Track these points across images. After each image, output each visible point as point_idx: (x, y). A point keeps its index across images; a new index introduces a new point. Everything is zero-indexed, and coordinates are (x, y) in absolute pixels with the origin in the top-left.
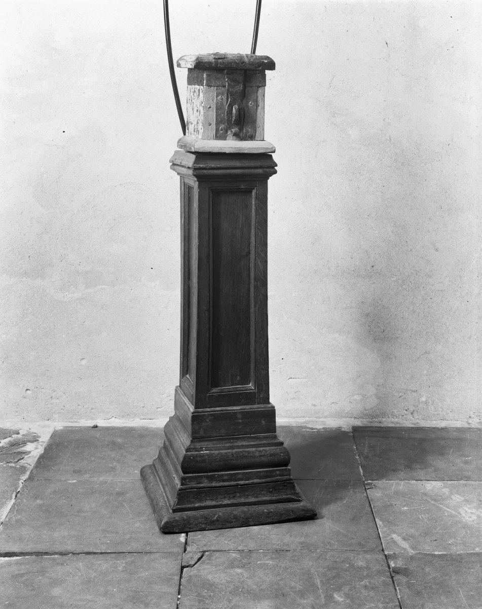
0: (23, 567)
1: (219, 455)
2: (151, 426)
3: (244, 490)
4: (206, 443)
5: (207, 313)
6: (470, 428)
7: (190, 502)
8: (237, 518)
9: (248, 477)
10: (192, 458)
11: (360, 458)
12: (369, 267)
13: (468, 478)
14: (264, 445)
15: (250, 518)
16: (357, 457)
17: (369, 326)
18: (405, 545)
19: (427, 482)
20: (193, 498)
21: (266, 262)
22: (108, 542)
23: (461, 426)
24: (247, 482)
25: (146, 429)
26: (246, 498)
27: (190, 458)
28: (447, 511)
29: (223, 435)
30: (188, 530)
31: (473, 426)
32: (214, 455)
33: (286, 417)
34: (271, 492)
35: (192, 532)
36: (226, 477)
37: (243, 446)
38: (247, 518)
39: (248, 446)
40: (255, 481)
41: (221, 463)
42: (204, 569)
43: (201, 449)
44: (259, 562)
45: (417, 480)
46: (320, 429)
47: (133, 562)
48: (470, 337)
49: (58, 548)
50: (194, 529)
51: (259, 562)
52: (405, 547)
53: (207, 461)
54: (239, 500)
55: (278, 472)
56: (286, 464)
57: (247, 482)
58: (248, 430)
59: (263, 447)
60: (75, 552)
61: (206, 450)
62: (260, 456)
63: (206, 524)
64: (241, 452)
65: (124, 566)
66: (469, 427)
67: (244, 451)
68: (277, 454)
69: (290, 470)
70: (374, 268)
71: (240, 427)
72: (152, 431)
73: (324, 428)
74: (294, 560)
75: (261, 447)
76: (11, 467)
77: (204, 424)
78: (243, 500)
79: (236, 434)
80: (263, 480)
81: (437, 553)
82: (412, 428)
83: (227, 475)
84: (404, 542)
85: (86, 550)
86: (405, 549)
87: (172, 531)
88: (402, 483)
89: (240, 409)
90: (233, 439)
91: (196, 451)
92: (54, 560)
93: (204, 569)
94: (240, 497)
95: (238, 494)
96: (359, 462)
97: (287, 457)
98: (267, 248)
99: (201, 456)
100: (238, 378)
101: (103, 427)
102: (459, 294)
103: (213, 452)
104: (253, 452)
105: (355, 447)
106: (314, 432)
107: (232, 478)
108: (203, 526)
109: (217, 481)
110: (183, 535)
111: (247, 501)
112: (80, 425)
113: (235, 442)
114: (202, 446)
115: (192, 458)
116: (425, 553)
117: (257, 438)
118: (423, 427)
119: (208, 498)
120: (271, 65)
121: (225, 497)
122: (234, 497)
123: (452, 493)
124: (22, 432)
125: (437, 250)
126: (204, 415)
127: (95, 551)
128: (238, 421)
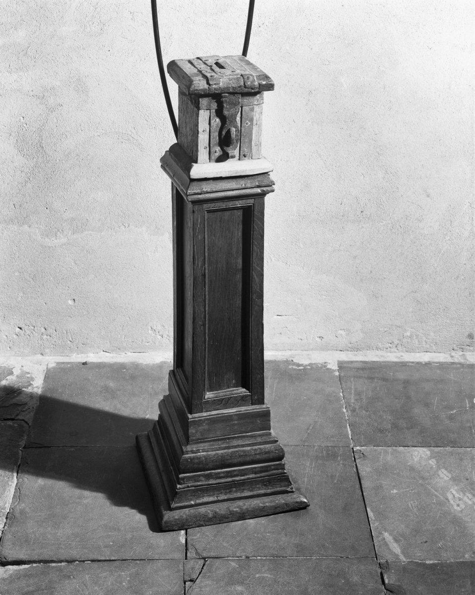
0: (31, 581)
1: (216, 456)
2: (141, 361)
3: (240, 485)
4: (202, 445)
5: (202, 327)
6: (453, 363)
7: (188, 499)
8: (233, 514)
9: (242, 472)
10: (189, 460)
11: (347, 411)
12: (359, 213)
13: (454, 444)
14: (260, 444)
15: (246, 513)
16: (345, 410)
17: (357, 267)
18: (396, 548)
19: (414, 448)
20: (191, 496)
21: (262, 275)
22: (111, 543)
23: (444, 361)
24: (243, 478)
25: (136, 366)
26: (242, 492)
27: (187, 461)
28: (436, 496)
29: (219, 435)
30: (186, 527)
31: (456, 361)
32: (211, 456)
33: (273, 350)
34: (265, 485)
35: (191, 528)
36: (222, 475)
37: (238, 446)
38: (243, 513)
39: (243, 446)
40: (251, 476)
41: (218, 463)
42: (206, 586)
43: (198, 451)
44: (257, 576)
45: (404, 446)
46: (306, 365)
47: (137, 574)
48: (458, 277)
49: (64, 554)
50: (193, 526)
51: (257, 576)
52: (396, 553)
53: (204, 462)
54: (235, 494)
55: (273, 467)
56: (281, 458)
57: (243, 478)
58: (243, 430)
59: (259, 445)
60: (80, 560)
61: (203, 452)
62: (255, 454)
63: (204, 521)
64: (237, 451)
65: (129, 581)
66: (452, 361)
67: (240, 451)
68: (272, 452)
69: (284, 465)
70: (363, 214)
71: (236, 427)
72: (143, 369)
73: (310, 365)
74: (291, 573)
75: (256, 445)
76: (10, 426)
77: (200, 428)
78: (239, 495)
79: (232, 434)
80: (258, 475)
81: (428, 562)
82: (396, 363)
83: (223, 472)
84: (395, 545)
85: (92, 557)
86: (397, 556)
87: (171, 529)
88: (390, 449)
89: (237, 412)
90: (229, 439)
91: (193, 453)
92: (60, 570)
93: (206, 586)
94: (236, 491)
95: (234, 489)
96: (347, 418)
97: (281, 454)
98: (263, 261)
99: (198, 458)
100: (234, 381)
101: (93, 363)
102: (449, 238)
103: (209, 453)
104: (248, 451)
105: (342, 395)
106: (300, 370)
107: (228, 475)
108: (202, 523)
109: (213, 478)
110: (183, 532)
111: (243, 495)
112: (72, 361)
113: (231, 442)
114: (198, 449)
115: (189, 460)
116: (416, 562)
117: (252, 437)
118: (407, 362)
119: (205, 495)
120: (270, 87)
121: (221, 493)
122: (230, 492)
123: (439, 468)
124: (17, 372)
125: (428, 196)
126: (201, 420)
127: (100, 559)
128: (234, 422)
